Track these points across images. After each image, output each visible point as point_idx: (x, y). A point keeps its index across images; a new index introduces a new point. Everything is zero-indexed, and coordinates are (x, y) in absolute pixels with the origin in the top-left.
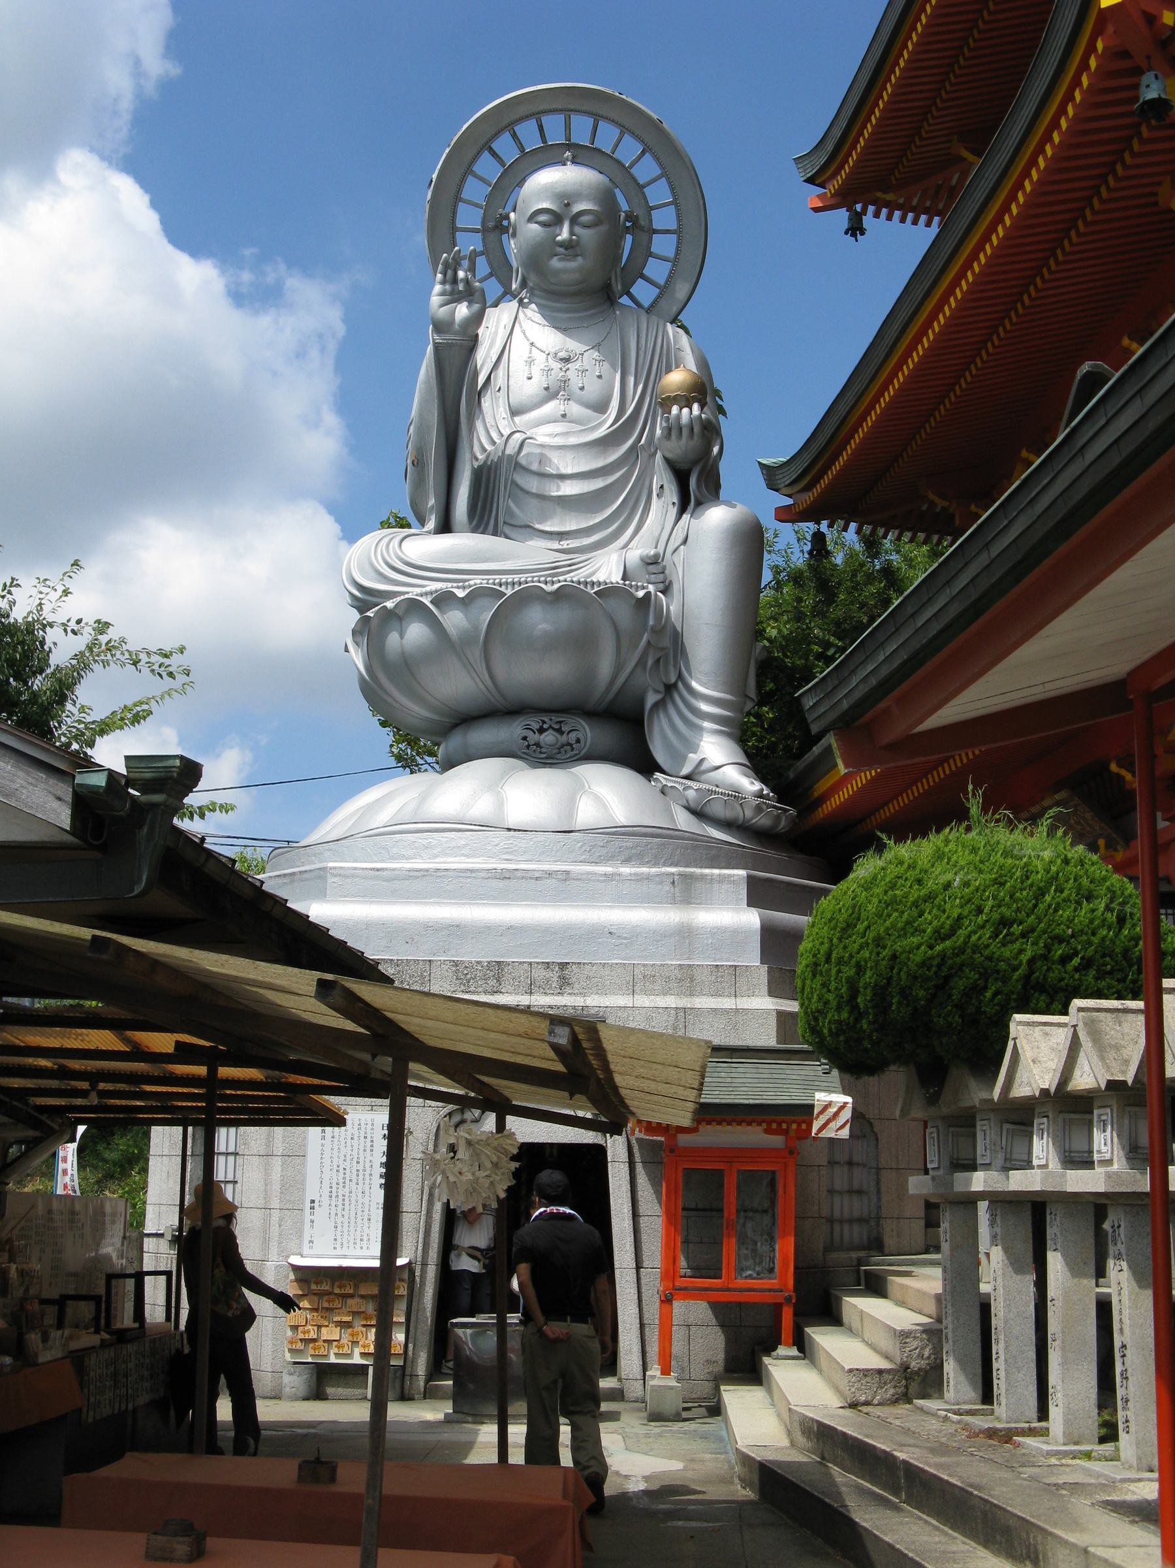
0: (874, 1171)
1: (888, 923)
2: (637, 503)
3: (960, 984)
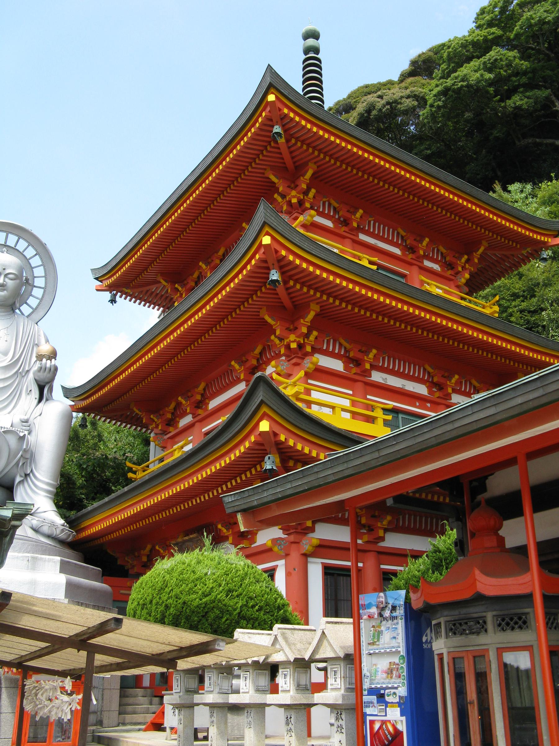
0: (101, 690)
1: (181, 589)
2: (15, 396)
3: (212, 615)
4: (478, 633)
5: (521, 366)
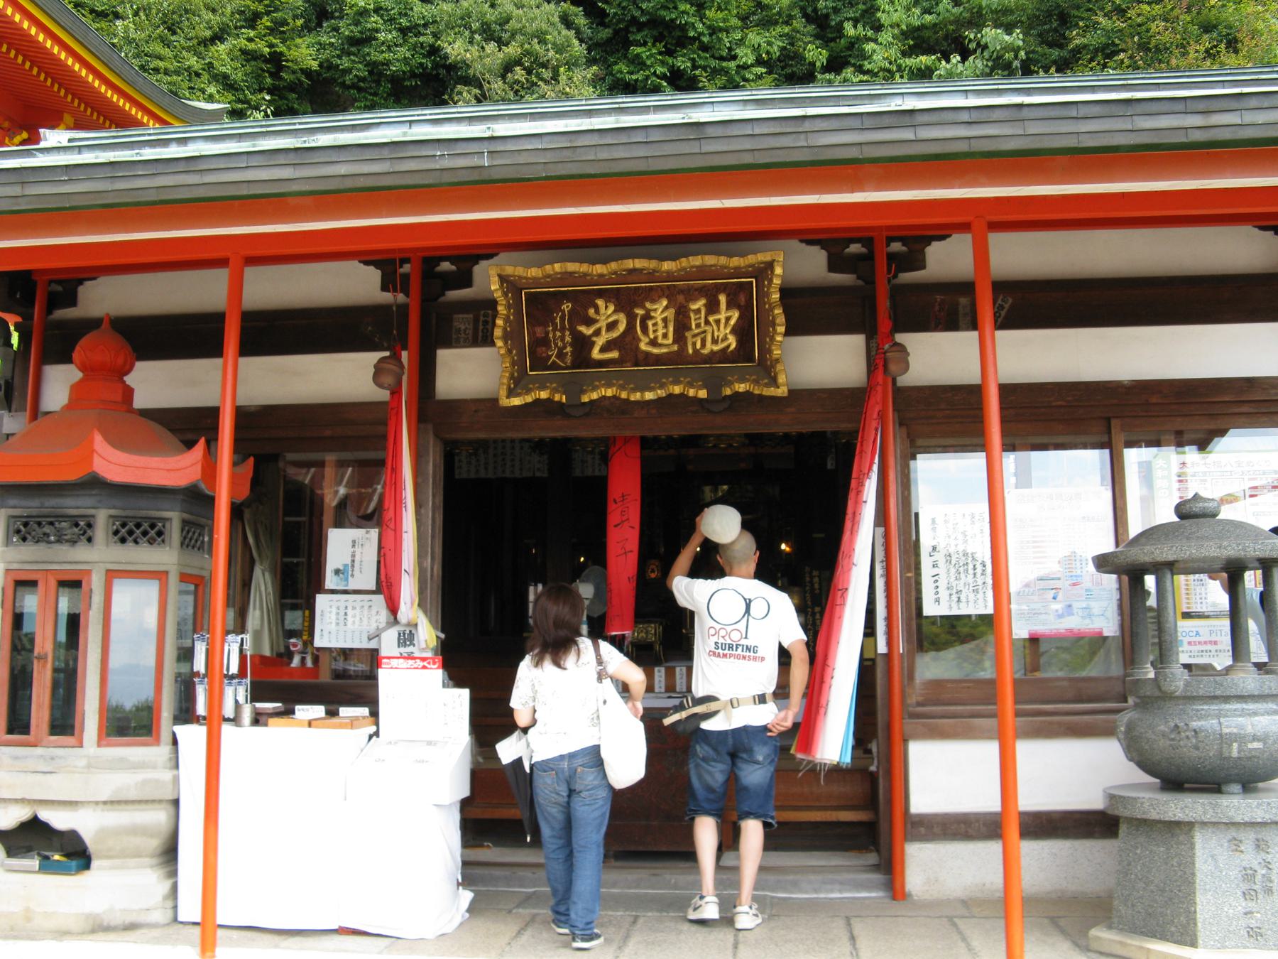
4: (73, 542)
5: (76, 104)
